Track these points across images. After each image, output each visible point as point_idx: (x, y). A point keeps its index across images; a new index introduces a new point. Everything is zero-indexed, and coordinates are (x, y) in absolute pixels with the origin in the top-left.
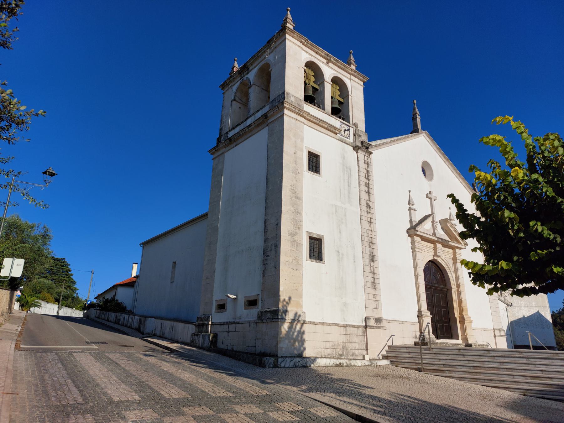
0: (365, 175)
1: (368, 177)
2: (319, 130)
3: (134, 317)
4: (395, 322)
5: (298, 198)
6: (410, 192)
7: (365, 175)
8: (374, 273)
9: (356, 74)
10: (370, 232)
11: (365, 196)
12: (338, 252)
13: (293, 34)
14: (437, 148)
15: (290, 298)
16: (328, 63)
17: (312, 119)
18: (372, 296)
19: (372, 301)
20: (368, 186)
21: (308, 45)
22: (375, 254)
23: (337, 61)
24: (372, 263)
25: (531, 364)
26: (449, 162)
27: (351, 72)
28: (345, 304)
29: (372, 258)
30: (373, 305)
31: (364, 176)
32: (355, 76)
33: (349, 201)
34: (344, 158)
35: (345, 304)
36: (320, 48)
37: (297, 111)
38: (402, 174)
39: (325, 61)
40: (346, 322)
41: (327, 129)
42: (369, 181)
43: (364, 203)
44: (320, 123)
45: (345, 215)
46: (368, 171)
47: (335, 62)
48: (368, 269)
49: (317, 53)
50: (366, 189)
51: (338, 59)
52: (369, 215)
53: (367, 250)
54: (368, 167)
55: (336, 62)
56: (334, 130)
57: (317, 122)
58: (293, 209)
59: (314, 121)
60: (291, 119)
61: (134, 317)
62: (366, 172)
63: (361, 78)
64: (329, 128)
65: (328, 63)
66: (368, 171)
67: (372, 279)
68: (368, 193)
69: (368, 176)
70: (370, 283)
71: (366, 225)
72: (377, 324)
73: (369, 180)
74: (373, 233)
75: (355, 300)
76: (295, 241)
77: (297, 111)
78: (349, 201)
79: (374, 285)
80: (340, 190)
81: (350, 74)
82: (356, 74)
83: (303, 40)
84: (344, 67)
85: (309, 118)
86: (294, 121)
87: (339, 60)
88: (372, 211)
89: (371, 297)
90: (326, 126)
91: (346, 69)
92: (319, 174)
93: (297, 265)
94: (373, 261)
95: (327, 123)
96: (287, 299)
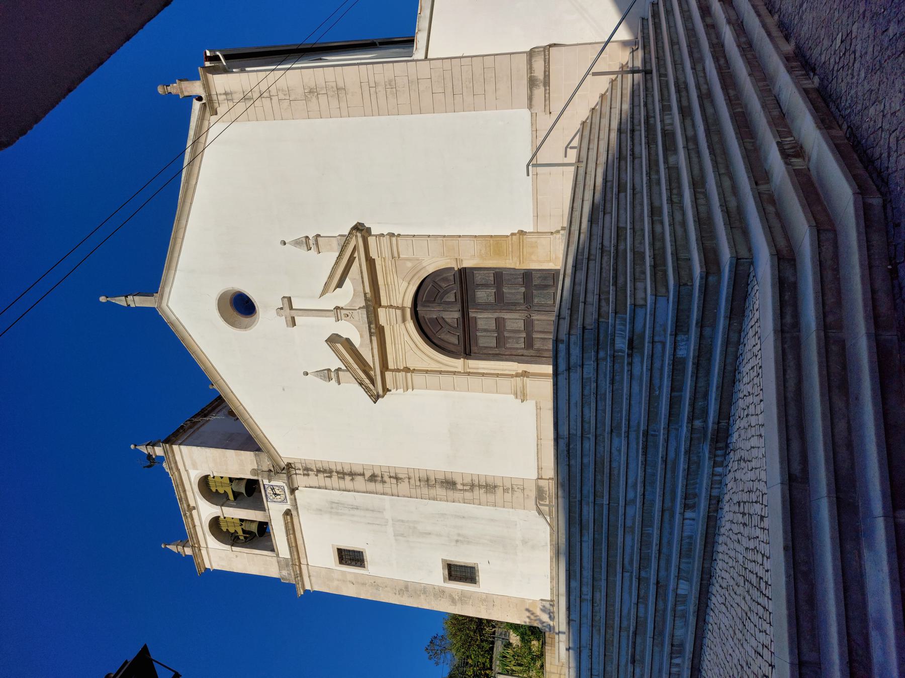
0: (327, 477)
1: (327, 472)
2: (302, 542)
3: (546, 354)
4: (540, 456)
5: (407, 588)
6: (306, 374)
7: (327, 477)
8: (472, 486)
9: (173, 465)
10: (412, 481)
11: (360, 482)
12: (457, 541)
13: (201, 564)
14: (169, 269)
15: (528, 610)
16: (194, 508)
17: (296, 557)
18: (506, 494)
19: (514, 497)
20: (342, 474)
21: (195, 541)
22: (441, 477)
23: (181, 500)
24: (459, 487)
25: (610, 112)
26: (176, 232)
27: (176, 473)
28: (525, 542)
29: (449, 484)
30: (518, 494)
31: (329, 479)
32: (176, 463)
33: (379, 512)
34: (320, 510)
35: (525, 542)
36: (186, 528)
37: (299, 578)
38: (284, 390)
39: (194, 512)
40: (547, 543)
41: (294, 533)
42: (333, 471)
43: (371, 486)
44: (294, 545)
45: (402, 521)
46: (319, 471)
47: (184, 502)
48: (468, 495)
49: (194, 526)
50: (348, 478)
51: (178, 500)
52: (386, 478)
53: (440, 491)
54: (312, 470)
55: (183, 500)
56: (290, 525)
57: (295, 549)
58: (422, 597)
59: (295, 553)
60: (312, 582)
61: (546, 354)
62: (321, 476)
63: (170, 454)
64: (291, 532)
65: (194, 508)
66: (319, 471)
67: (482, 491)
68: (352, 475)
69: (324, 471)
70: (488, 495)
71: (404, 487)
72: (546, 499)
73: (331, 472)
74: (412, 475)
75: (516, 525)
76: (461, 599)
77: (299, 578)
78: (379, 512)
79: (490, 488)
80: (369, 523)
81: (178, 470)
82: (173, 465)
83: (197, 551)
84: (180, 486)
85: (297, 560)
86: (313, 579)
87: (177, 497)
88: (378, 472)
89: (508, 496)
90: (292, 536)
91: (178, 482)
92: (364, 567)
93: (487, 599)
94: (454, 484)
95: (288, 539)
96: (528, 614)
